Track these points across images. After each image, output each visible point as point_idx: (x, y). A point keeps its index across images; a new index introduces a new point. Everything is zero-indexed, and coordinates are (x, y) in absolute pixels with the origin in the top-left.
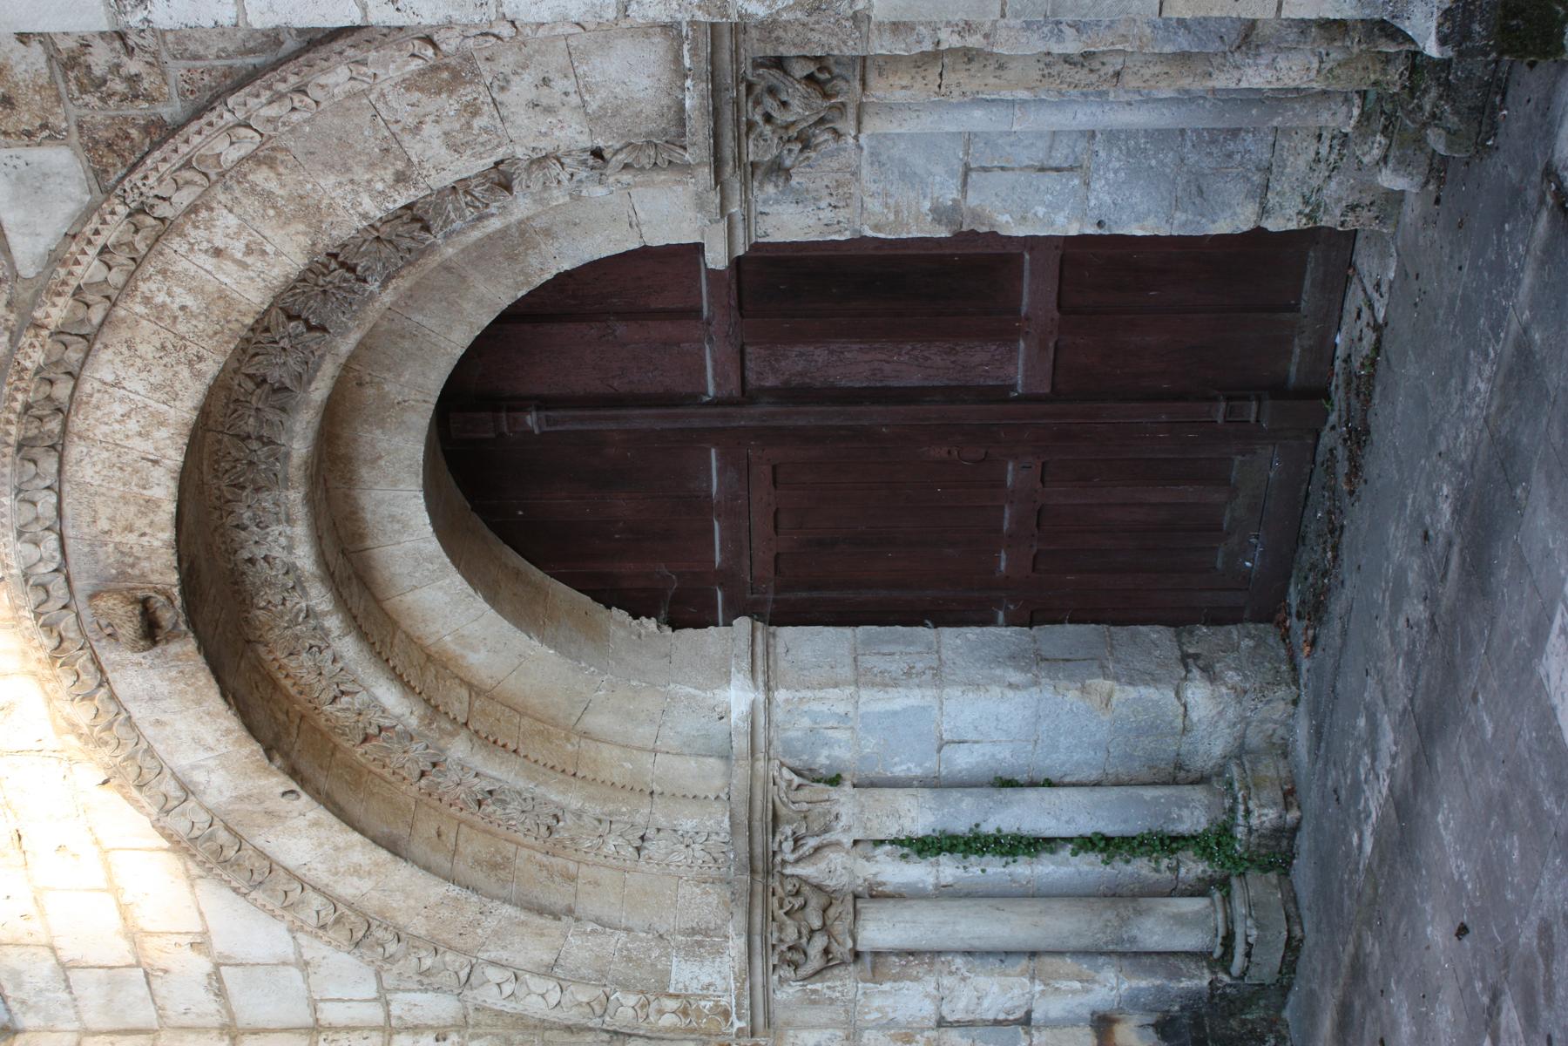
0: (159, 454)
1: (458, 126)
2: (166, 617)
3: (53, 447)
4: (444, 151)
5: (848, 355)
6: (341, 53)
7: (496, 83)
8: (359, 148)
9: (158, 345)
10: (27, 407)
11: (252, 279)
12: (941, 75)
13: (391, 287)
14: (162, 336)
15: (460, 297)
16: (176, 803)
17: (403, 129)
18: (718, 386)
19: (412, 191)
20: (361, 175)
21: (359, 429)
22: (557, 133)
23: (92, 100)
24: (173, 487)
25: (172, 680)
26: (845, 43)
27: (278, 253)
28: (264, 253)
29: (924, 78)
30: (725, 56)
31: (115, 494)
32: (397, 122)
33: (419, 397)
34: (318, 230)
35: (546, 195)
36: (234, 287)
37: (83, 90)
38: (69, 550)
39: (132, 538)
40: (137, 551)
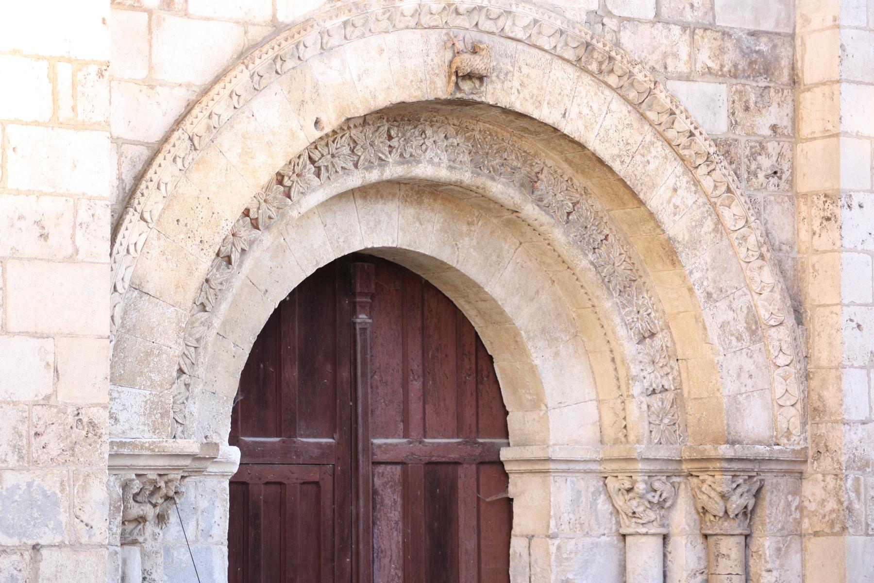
0: (569, 120)
1: (732, 329)
2: (466, 86)
3: (579, 60)
4: (721, 320)
5: (395, 533)
6: (779, 281)
7: (750, 351)
8: (722, 277)
9: (629, 141)
10: (611, 58)
11: (662, 204)
12: (737, 574)
13: (591, 267)
14: (634, 146)
15: (521, 296)
16: (324, 41)
17: (731, 302)
18: (380, 446)
19: (703, 300)
20: (711, 275)
21: (440, 215)
22: (729, 378)
23: (747, 152)
24: (549, 121)
25: (415, 72)
26: (772, 525)
27: (674, 222)
28: (675, 214)
29: (736, 565)
30: (773, 466)
31: (544, 84)
32: (734, 299)
33: (461, 259)
34: (685, 246)
35: (637, 362)
36: (658, 193)
37: (751, 147)
38: (509, 41)
39: (516, 84)
40: (507, 84)
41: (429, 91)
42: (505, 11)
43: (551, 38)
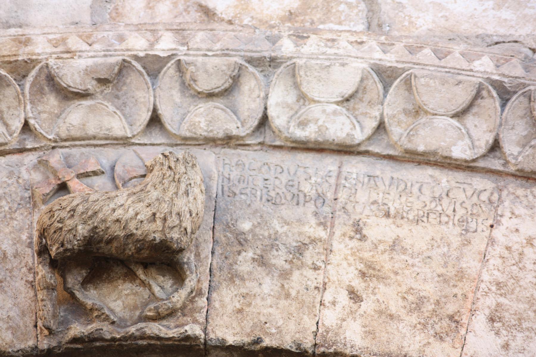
42: (250, 61)
43: (470, 120)
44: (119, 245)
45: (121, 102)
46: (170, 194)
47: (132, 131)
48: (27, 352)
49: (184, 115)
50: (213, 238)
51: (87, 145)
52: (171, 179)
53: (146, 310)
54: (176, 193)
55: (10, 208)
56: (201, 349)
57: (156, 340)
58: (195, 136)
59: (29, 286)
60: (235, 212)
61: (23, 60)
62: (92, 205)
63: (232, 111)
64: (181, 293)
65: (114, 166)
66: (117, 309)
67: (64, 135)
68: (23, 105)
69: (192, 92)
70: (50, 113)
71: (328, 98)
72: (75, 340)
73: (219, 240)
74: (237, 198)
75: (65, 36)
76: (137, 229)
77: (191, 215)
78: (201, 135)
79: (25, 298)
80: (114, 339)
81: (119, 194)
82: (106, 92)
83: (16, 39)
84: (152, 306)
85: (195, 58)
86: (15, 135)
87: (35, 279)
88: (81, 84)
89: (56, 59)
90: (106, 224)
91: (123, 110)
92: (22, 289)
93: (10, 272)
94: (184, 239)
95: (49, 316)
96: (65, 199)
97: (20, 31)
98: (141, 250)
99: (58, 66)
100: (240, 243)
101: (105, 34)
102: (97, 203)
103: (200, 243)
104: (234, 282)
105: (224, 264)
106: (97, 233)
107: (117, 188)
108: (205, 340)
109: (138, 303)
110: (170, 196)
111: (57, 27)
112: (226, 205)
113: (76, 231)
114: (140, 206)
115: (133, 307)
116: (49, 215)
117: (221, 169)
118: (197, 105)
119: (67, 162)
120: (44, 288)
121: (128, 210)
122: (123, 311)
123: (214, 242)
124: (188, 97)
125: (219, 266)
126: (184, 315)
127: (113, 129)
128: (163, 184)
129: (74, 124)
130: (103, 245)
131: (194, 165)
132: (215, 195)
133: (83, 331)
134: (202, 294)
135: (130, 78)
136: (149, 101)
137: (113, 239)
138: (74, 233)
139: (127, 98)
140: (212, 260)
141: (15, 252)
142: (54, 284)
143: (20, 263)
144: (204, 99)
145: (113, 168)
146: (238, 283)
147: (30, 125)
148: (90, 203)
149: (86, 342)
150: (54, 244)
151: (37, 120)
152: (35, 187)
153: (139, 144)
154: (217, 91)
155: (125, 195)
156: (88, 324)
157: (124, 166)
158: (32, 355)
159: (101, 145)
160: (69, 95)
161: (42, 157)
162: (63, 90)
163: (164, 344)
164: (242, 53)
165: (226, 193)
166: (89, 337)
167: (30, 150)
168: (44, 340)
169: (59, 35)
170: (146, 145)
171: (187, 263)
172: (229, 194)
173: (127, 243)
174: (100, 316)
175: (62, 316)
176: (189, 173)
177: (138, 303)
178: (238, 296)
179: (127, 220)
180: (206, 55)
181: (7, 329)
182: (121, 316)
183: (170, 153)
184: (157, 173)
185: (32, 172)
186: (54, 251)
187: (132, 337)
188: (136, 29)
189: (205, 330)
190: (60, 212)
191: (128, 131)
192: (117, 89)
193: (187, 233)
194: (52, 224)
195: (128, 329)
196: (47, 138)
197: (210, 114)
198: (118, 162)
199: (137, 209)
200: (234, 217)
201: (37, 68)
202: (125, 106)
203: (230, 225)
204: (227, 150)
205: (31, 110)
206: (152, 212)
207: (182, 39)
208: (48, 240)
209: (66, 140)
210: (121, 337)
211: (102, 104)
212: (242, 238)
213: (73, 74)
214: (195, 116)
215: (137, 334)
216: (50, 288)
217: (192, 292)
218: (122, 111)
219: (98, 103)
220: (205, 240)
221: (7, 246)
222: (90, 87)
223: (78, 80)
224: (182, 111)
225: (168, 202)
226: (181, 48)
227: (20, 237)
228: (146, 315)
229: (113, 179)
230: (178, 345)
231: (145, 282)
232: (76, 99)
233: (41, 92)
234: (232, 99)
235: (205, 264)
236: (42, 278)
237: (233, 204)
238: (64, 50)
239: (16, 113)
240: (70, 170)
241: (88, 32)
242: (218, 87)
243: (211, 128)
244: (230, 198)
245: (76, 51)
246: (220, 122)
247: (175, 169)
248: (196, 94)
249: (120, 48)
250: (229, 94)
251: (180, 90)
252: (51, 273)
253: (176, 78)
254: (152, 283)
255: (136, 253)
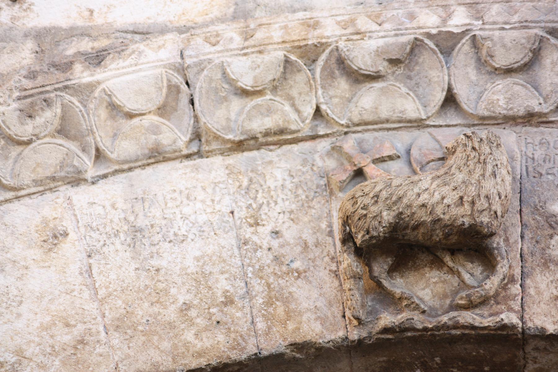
41: (261, 325)
44: (426, 231)
45: (413, 82)
46: (476, 176)
47: (426, 113)
48: (338, 343)
49: (480, 93)
50: (521, 221)
51: (380, 129)
52: (476, 160)
53: (457, 299)
54: (483, 175)
55: (307, 197)
56: (519, 339)
57: (470, 330)
58: (494, 115)
59: (333, 275)
60: (542, 194)
61: (313, 44)
62: (395, 190)
63: (532, 86)
64: (493, 280)
65: (410, 150)
66: (427, 298)
67: (356, 120)
68: (314, 90)
69: (489, 68)
70: (341, 98)
71: (107, 148)
72: (386, 330)
73: (528, 223)
74: (544, 179)
75: (353, 17)
76: (444, 214)
77: (500, 198)
78: (500, 113)
79: (330, 287)
80: (425, 329)
81: (422, 178)
82: (397, 73)
83: (304, 22)
84: (464, 294)
85: (491, 33)
86: (308, 121)
87: (338, 269)
88: (372, 66)
89: (346, 41)
90: (411, 210)
91: (415, 91)
92: (327, 279)
93: (313, 262)
94: (495, 223)
95: (358, 306)
96: (367, 186)
97: (308, 14)
98: (449, 235)
99: (348, 48)
100: (551, 226)
101: (395, 12)
102: (400, 188)
103: (508, 227)
104: (548, 267)
105: (535, 249)
106: (402, 219)
107: (415, 172)
108: (523, 328)
109: (448, 291)
110: (477, 178)
111: (344, 8)
112: (533, 187)
113: (381, 217)
114: (445, 190)
115: (443, 295)
116: (352, 202)
117: (524, 149)
118: (494, 83)
119: (361, 148)
120: (351, 277)
121: (433, 195)
122: (433, 299)
123: (522, 225)
124: (484, 74)
125: (530, 251)
126: (498, 303)
127: (407, 111)
128: (468, 166)
129: (366, 108)
130: (409, 231)
131: (498, 145)
132: (519, 176)
133: (393, 320)
134: (515, 281)
135: (422, 57)
136: (443, 80)
137: (420, 224)
138: (379, 220)
139: (420, 78)
140: (522, 245)
141: (315, 241)
142: (361, 273)
143: (322, 252)
144: (502, 76)
145: (408, 152)
146: (553, 268)
147: (322, 110)
148: (394, 188)
149: (397, 332)
150: (359, 232)
151: (328, 105)
152: (331, 174)
153: (434, 126)
154: (516, 66)
155: (428, 178)
156: (397, 313)
157: (420, 150)
158: (343, 346)
159: (394, 129)
160: (359, 78)
161: (336, 143)
162: (353, 73)
163: (479, 334)
164: (543, 25)
165: (532, 174)
166: (400, 327)
167: (322, 136)
168: (354, 330)
169: (348, 16)
170: (441, 126)
171: (497, 249)
172: (534, 175)
173: (434, 228)
174: (410, 305)
175: (370, 306)
176: (494, 153)
177: (448, 291)
178: (554, 282)
179: (433, 205)
180: (503, 29)
181: (316, 319)
182: (431, 305)
183: (473, 133)
184: (460, 155)
185: (326, 159)
186: (359, 238)
187: (445, 326)
188: (426, 5)
189: (522, 318)
190: (363, 198)
191: (422, 113)
192: (409, 70)
193: (497, 216)
194: (356, 211)
195: (440, 319)
196: (340, 124)
197: (509, 91)
198: (414, 145)
199: (443, 193)
200: (542, 198)
201: (327, 51)
202: (418, 87)
203: (539, 207)
204: (529, 129)
205: (322, 95)
206: (458, 196)
207: (477, 13)
208: (352, 227)
209: (358, 125)
210: (434, 326)
211: (394, 85)
212: (553, 221)
213: (364, 56)
214: (493, 93)
215: (450, 323)
216: (356, 277)
217: (504, 279)
218: (415, 92)
219: (390, 85)
220: (512, 224)
221: (307, 235)
222: (381, 68)
223: (369, 62)
224: (478, 89)
225: (475, 185)
226: (476, 23)
227: (319, 226)
228: (458, 304)
229: (410, 163)
230: (494, 334)
231: (453, 269)
232: (367, 81)
233: (332, 76)
234: (532, 74)
235: (515, 249)
236: (349, 267)
237: (540, 185)
238: (354, 31)
239: (308, 98)
240: (365, 155)
241: (377, 11)
242: (517, 62)
243: (511, 106)
244: (536, 179)
245: (366, 32)
246: (520, 99)
247: (480, 149)
248: (493, 70)
249: (411, 26)
250: (529, 69)
251: (476, 67)
252: (357, 261)
253: (471, 55)
254: (460, 269)
255: (444, 238)
